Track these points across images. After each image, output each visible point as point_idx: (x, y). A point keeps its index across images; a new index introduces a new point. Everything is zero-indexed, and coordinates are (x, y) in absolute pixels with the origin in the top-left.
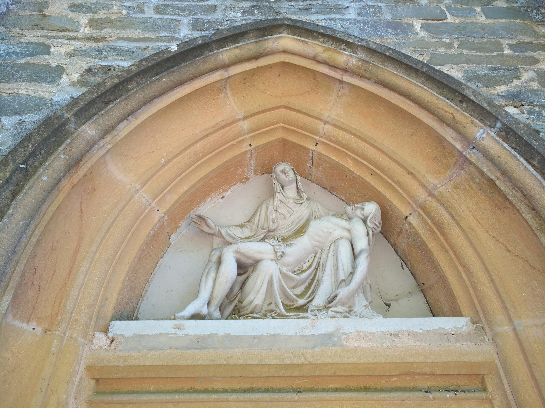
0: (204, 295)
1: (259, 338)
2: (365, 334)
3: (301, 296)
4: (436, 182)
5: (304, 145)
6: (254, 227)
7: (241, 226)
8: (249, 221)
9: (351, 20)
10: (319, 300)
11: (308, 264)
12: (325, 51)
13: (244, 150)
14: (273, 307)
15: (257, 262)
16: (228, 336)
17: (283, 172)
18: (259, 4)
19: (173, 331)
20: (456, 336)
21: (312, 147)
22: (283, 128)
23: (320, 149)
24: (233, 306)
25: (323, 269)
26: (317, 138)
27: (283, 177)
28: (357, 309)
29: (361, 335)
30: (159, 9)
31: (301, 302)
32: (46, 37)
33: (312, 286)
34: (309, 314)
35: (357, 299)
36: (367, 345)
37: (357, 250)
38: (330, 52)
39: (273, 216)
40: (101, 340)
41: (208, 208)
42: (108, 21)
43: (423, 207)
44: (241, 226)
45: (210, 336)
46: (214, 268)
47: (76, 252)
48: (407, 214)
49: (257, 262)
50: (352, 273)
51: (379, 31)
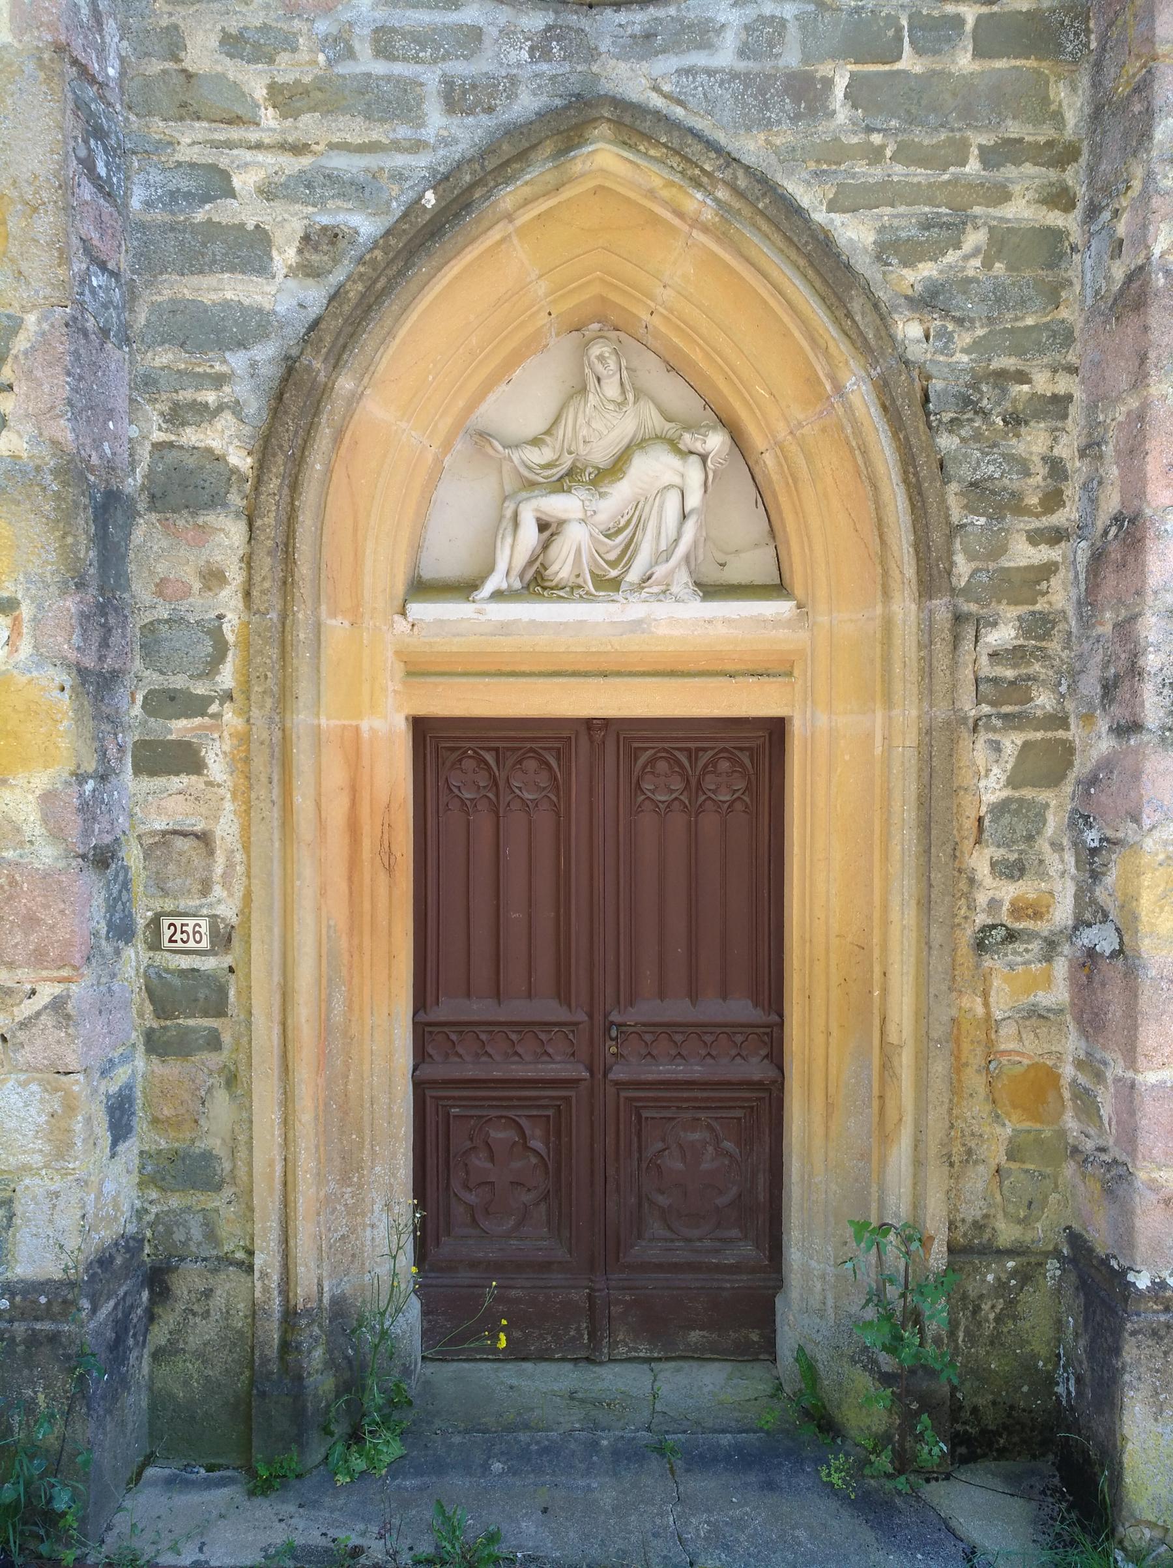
0: (501, 566)
1: (565, 624)
2: (677, 620)
3: (612, 564)
4: (801, 417)
5: (635, 311)
6: (558, 446)
7: (536, 442)
8: (548, 432)
9: (723, 71)
10: (633, 576)
11: (626, 518)
12: (665, 186)
13: (540, 323)
14: (580, 581)
15: (562, 523)
16: (532, 622)
17: (601, 358)
18: (560, 22)
19: (475, 616)
20: (776, 623)
21: (645, 316)
22: (602, 280)
23: (656, 321)
24: (537, 582)
25: (644, 529)
26: (652, 304)
27: (599, 368)
28: (674, 589)
29: (673, 621)
30: (385, 42)
31: (614, 573)
32: (217, 145)
33: (628, 551)
34: (619, 596)
35: (676, 576)
36: (676, 632)
37: (687, 510)
38: (674, 190)
39: (584, 432)
40: (401, 625)
41: (490, 412)
42: (301, 90)
43: (779, 445)
44: (536, 442)
45: (515, 622)
46: (510, 529)
47: (355, 530)
48: (762, 449)
49: (562, 523)
50: (676, 541)
51: (768, 110)
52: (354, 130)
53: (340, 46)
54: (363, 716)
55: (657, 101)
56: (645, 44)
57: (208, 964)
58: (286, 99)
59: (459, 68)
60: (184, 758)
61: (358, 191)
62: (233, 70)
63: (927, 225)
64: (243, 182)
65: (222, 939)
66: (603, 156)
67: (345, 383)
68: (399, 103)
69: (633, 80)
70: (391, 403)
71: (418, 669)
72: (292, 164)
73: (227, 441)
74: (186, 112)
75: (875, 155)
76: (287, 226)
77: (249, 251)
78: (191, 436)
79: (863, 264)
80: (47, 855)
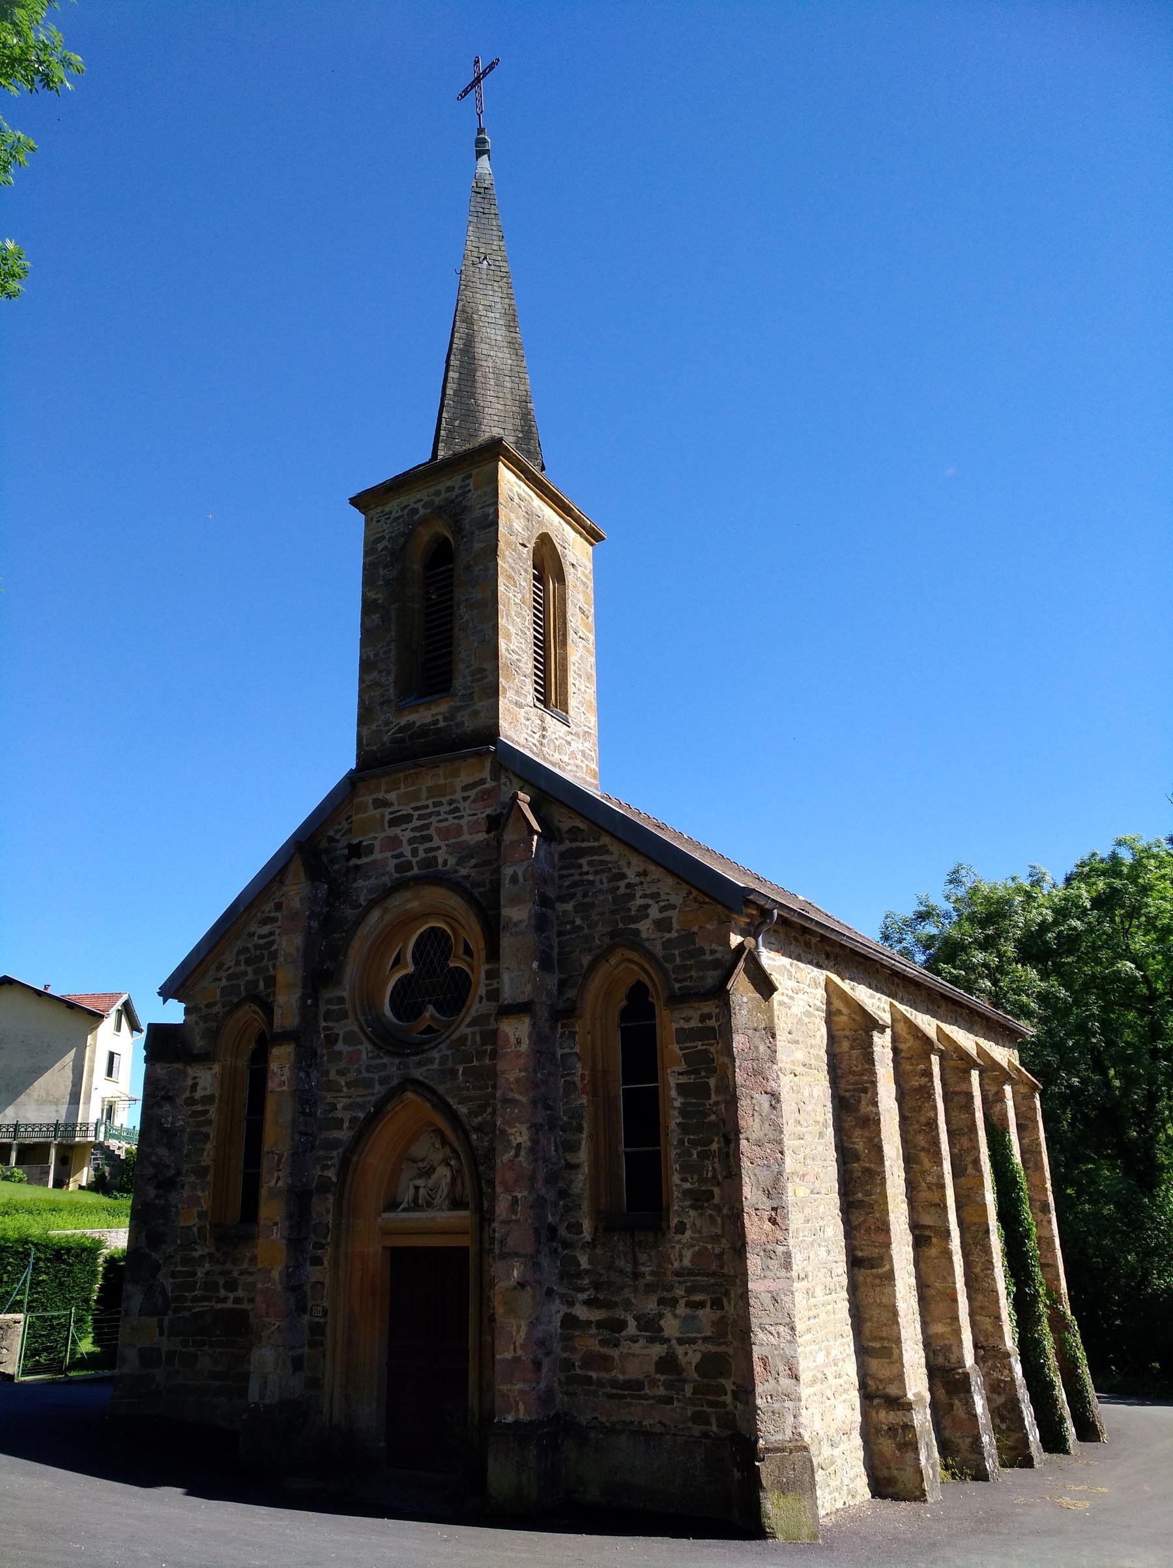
24: (415, 1206)
52: (361, 1091)
53: (359, 1071)
54: (369, 1245)
55: (421, 1078)
56: (419, 1065)
57: (321, 1320)
58: (349, 1085)
59: (382, 1074)
60: (317, 1261)
61: (361, 1107)
62: (338, 1078)
63: (479, 1107)
64: (339, 1106)
65: (325, 1312)
66: (410, 1095)
67: (355, 1159)
68: (368, 1084)
69: (418, 1074)
70: (377, 1157)
71: (386, 1233)
72: (349, 1101)
73: (331, 1174)
74: (329, 1090)
75: (467, 1089)
76: (346, 1116)
77: (338, 1124)
78: (326, 1173)
79: (464, 1119)
80: (279, 1287)
